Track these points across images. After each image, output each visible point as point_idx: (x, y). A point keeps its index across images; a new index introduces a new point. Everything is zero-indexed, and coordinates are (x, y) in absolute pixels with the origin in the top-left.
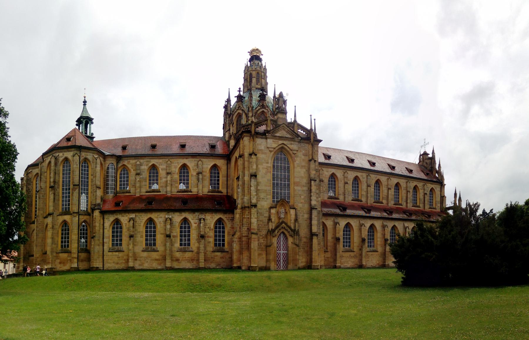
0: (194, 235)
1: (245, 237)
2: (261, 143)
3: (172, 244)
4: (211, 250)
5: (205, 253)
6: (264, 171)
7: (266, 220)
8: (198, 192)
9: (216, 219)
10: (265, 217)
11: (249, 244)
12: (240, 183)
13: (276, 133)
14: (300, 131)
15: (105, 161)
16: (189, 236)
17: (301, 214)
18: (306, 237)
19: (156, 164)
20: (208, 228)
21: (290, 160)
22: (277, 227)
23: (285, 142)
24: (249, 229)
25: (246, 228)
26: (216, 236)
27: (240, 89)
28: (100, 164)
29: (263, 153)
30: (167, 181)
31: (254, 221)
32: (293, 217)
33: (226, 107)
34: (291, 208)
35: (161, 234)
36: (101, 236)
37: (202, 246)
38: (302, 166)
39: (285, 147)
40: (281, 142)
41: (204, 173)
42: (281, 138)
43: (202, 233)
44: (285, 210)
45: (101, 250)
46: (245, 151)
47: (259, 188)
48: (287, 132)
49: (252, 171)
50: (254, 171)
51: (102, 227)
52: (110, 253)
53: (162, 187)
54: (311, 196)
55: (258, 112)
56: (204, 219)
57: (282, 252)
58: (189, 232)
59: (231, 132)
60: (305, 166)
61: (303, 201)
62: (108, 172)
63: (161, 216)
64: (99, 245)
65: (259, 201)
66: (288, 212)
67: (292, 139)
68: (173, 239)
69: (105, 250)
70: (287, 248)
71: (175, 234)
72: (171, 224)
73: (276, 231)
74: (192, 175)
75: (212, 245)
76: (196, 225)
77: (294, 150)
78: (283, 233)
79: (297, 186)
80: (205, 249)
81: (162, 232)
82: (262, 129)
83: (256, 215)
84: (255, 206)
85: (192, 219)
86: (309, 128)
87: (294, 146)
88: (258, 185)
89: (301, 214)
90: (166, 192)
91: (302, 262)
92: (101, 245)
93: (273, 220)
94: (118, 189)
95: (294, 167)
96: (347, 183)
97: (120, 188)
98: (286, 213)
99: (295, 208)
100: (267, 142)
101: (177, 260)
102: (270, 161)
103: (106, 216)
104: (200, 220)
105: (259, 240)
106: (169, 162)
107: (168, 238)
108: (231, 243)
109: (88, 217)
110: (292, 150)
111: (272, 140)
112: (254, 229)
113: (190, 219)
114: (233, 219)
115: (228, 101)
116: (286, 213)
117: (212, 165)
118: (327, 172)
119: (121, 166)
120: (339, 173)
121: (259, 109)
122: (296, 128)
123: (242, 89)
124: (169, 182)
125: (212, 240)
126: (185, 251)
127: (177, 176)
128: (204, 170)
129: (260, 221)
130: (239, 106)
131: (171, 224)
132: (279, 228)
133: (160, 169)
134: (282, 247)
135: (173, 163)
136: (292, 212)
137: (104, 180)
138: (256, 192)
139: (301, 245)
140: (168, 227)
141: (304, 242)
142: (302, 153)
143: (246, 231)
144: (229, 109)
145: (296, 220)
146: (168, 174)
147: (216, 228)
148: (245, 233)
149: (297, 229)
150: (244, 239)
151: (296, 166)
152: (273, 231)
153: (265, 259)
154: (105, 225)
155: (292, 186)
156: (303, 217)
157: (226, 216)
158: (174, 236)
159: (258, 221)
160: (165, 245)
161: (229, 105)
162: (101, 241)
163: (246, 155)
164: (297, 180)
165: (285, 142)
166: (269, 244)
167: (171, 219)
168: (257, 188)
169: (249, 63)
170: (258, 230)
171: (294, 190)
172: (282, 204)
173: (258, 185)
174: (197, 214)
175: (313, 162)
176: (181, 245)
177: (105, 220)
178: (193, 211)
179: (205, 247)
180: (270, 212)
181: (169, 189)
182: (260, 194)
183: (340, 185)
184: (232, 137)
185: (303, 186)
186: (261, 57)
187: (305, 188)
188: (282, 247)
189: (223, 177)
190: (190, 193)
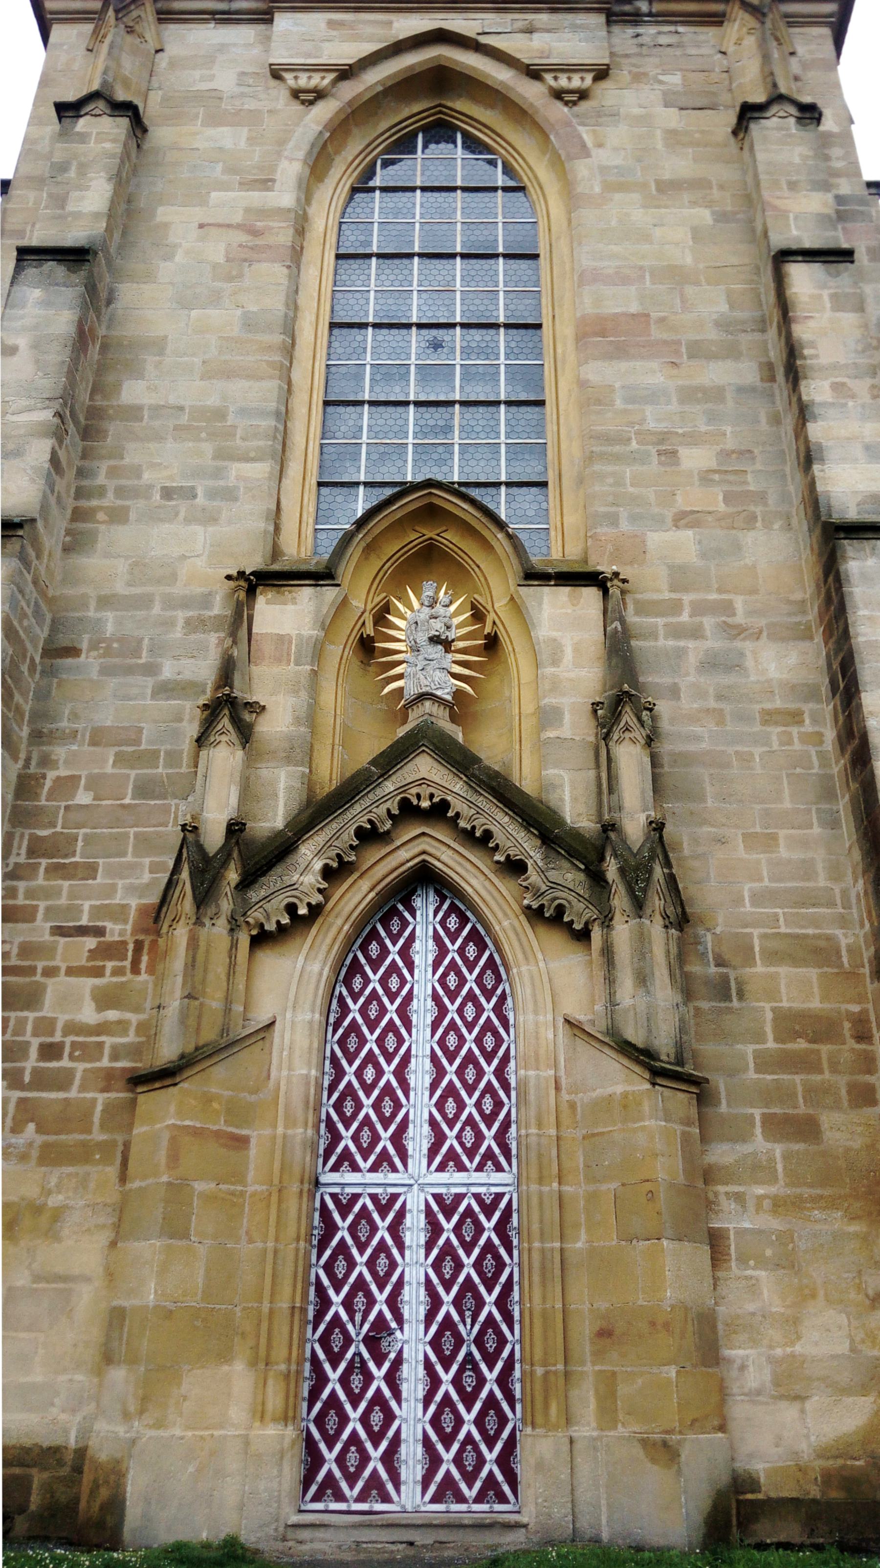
10: (165, 690)
17: (695, 651)
29: (215, 120)
38: (668, 188)
54: (803, 413)
57: (418, 1183)
70: (480, 1124)
78: (424, 877)
89: (695, 651)
91: (791, 1384)
93: (278, 721)
110: (534, 73)
116: (492, 644)
132: (358, 814)
134: (420, 1106)
139: (741, 1061)
141: (791, 1024)
145: (623, 703)
149: (634, 827)
152: (260, 857)
153: (87, 1298)
180: (240, 620)
187: (738, 372)
188: (420, 1106)
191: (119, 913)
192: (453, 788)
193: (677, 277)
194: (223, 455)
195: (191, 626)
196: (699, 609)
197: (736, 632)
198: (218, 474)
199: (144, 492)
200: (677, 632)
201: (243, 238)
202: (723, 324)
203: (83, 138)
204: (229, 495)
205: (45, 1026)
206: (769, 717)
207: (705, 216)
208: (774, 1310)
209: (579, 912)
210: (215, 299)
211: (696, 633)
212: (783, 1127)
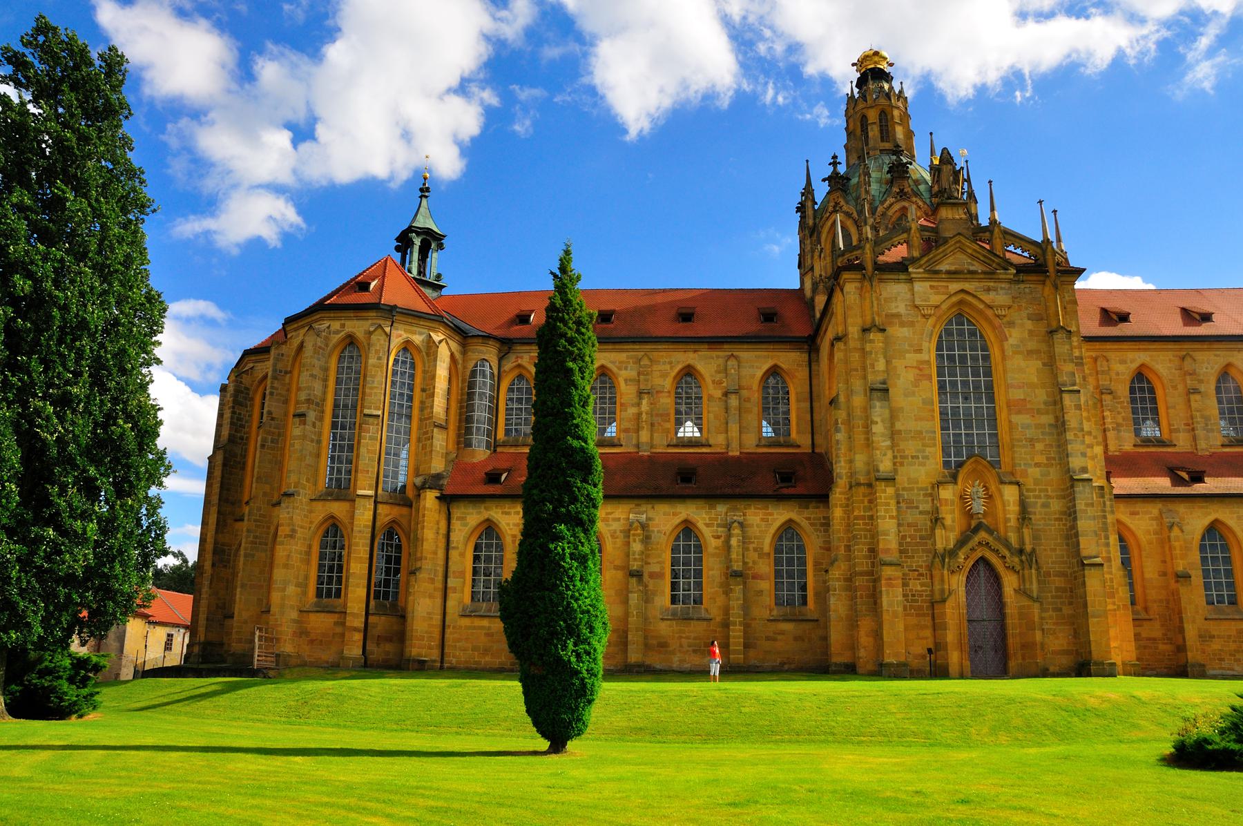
0: (712, 570)
1: (862, 574)
2: (895, 295)
3: (647, 598)
4: (766, 614)
5: (747, 626)
6: (911, 375)
7: (924, 521)
8: (728, 446)
9: (777, 524)
10: (921, 513)
11: (874, 598)
12: (841, 415)
13: (939, 262)
14: (1011, 248)
15: (464, 353)
16: (699, 574)
17: (1040, 501)
18: (1062, 574)
19: (609, 365)
20: (755, 550)
21: (990, 335)
22: (961, 543)
23: (967, 286)
24: (873, 551)
25: (865, 548)
26: (778, 574)
27: (835, 157)
28: (448, 360)
29: (902, 325)
30: (639, 414)
31: (888, 526)
32: (1013, 509)
33: (801, 208)
34: (1002, 482)
35: (616, 568)
36: (441, 570)
37: (736, 604)
38: (1030, 352)
39: (969, 299)
40: (954, 287)
41: (745, 393)
42: (954, 275)
43: (737, 566)
44: (986, 488)
45: (439, 611)
46: (850, 321)
47: (898, 426)
48: (972, 256)
49: (874, 379)
50: (880, 378)
51: (442, 545)
52: (466, 622)
53: (626, 431)
55: (890, 213)
56: (741, 525)
58: (699, 561)
59: (817, 271)
60: (1038, 352)
61: (1041, 459)
62: (471, 385)
63: (616, 515)
64: (431, 596)
65: (902, 464)
66: (996, 495)
67: (990, 275)
68: (651, 584)
69: (449, 610)
71: (655, 568)
72: (646, 539)
73: (962, 556)
74: (710, 397)
75: (769, 600)
76: (719, 542)
77: (1001, 307)
78: (982, 559)
79: (1019, 412)
80: (746, 615)
81: (618, 563)
82: (897, 253)
83: (893, 507)
84: (890, 480)
85: (707, 525)
86: (1039, 239)
87: (999, 296)
88: (893, 417)
89: (1040, 501)
90: (638, 446)
92: (439, 595)
93: (948, 522)
94: (501, 435)
95: (1004, 358)
96: (1196, 391)
97: (508, 432)
98: (990, 497)
99: (1018, 483)
100: (912, 290)
101: (663, 645)
102: (925, 345)
103: (458, 511)
104: (729, 527)
105: (905, 585)
106: (645, 362)
107: (634, 581)
108: (823, 594)
109: (405, 510)
110: (990, 307)
111: (927, 284)
112: (887, 551)
113: (700, 525)
114: (826, 524)
115: (808, 191)
116: (990, 497)
117: (766, 367)
118: (1123, 362)
119: (511, 370)
120: (1162, 363)
121: (891, 205)
122: (998, 242)
123: (842, 158)
124: (644, 416)
125: (766, 586)
126: (687, 618)
127: (667, 401)
128: (744, 383)
129: (909, 525)
130: (837, 204)
131: (646, 539)
132: (970, 545)
133: (621, 381)
135: (658, 362)
136: (1010, 494)
137: (461, 407)
138: (892, 439)
140: (637, 547)
141: (1057, 589)
142: (1024, 314)
143: (866, 557)
144: (810, 212)
146: (640, 393)
147: (778, 550)
148: (863, 565)
149: (1028, 548)
150: (860, 581)
151: (1009, 352)
154: (453, 537)
155: (1002, 416)
156: (1047, 509)
157: (806, 513)
158: (652, 575)
159: (899, 525)
160: (626, 602)
161: (809, 204)
162: (439, 585)
163: (854, 331)
164: (1017, 394)
165: (967, 286)
166: (937, 597)
167: (644, 526)
168: (892, 425)
169: (856, 90)
170: (901, 552)
171: (1012, 427)
172: (974, 470)
173: (893, 417)
174: (721, 508)
175: (1059, 337)
176: (674, 600)
177: (454, 521)
178: (711, 496)
179: (746, 607)
181: (644, 436)
182: (902, 445)
183: (1169, 399)
184: (821, 287)
185: (1039, 412)
186: (883, 66)
189: (798, 401)
190: (704, 450)
191: (921, 567)
192: (990, 539)
193: (1031, 386)
194: (924, 445)
195: (925, 495)
196: (1040, 491)
197: (1048, 497)
198: (924, 451)
199: (907, 457)
200: (1035, 497)
201: (917, 371)
202: (1045, 403)
203: (872, 341)
204: (927, 457)
205: (911, 590)
206: (1056, 519)
207: (1039, 363)
208: (1018, 93)
209: (1018, 568)
210: (913, 394)
211: (1039, 497)
212: (1055, 610)
